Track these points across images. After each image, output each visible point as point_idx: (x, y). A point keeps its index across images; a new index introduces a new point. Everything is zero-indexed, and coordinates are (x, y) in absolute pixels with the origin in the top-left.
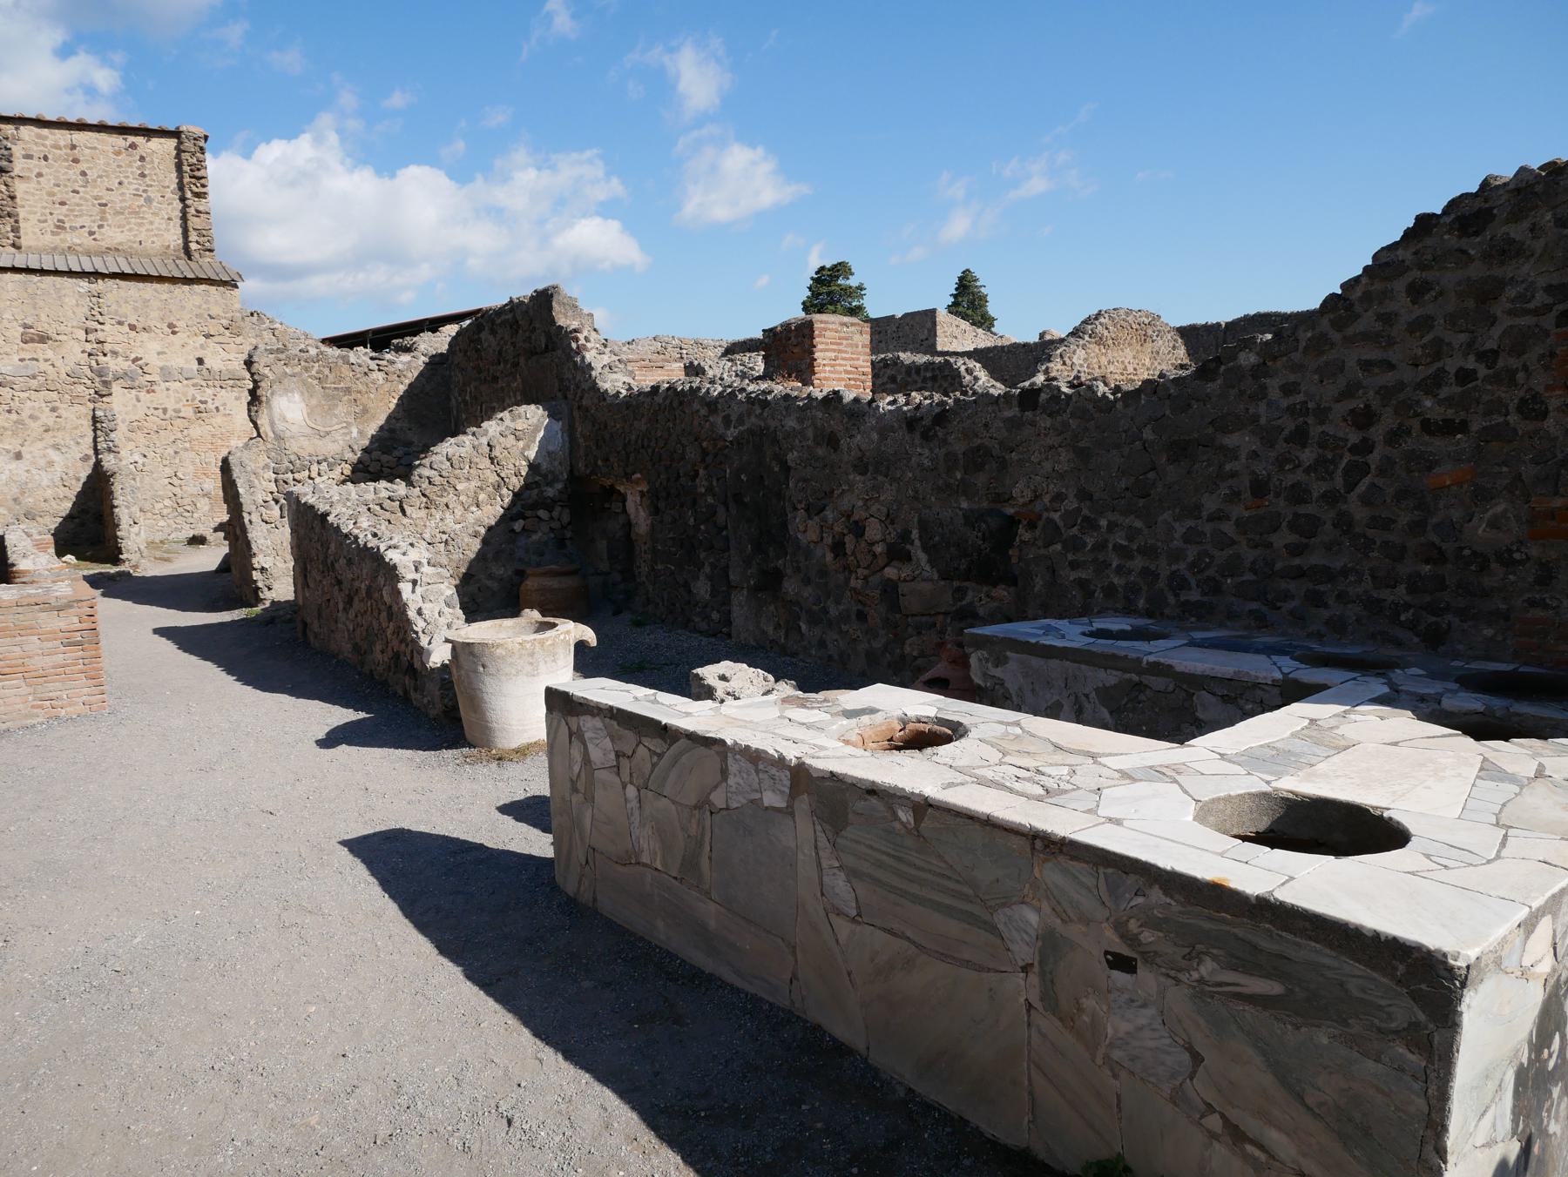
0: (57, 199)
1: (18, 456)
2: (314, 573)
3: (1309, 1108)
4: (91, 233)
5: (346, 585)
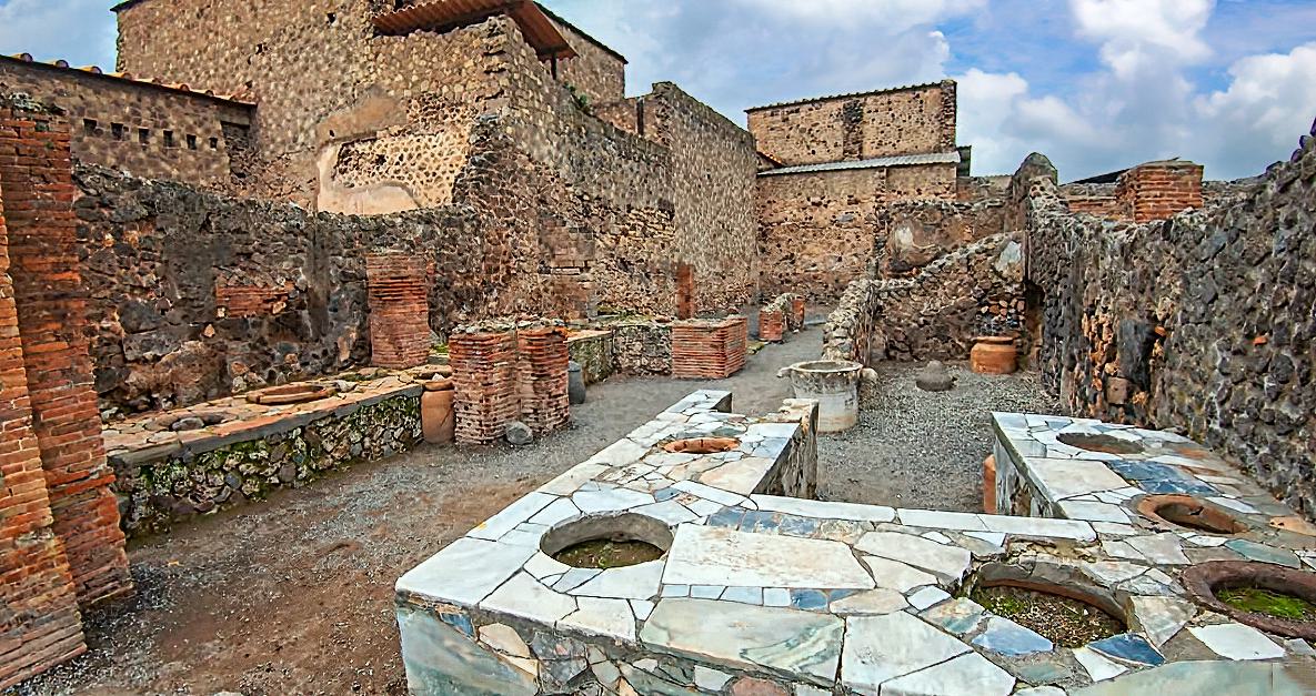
1: (840, 260)
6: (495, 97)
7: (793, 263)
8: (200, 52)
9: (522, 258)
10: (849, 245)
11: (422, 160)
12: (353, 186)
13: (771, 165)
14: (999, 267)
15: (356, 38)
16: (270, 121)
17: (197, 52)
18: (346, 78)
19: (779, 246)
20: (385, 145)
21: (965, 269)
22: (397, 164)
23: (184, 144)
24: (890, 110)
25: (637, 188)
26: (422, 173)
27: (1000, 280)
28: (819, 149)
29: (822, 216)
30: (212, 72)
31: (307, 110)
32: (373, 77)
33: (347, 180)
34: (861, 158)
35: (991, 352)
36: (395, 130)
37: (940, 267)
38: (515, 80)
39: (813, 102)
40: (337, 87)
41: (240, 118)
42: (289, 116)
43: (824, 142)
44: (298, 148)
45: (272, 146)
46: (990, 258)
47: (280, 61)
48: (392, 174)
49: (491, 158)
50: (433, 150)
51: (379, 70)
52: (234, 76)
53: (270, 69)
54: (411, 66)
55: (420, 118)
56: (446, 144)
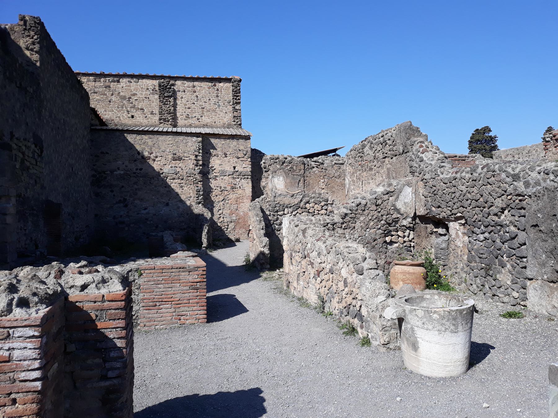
0: (187, 107)
1: (167, 204)
2: (297, 258)
5: (316, 265)
7: (126, 206)
14: (399, 205)
19: (112, 191)
24: (195, 92)
27: (399, 216)
28: (138, 114)
35: (414, 273)
39: (132, 76)
46: (391, 198)
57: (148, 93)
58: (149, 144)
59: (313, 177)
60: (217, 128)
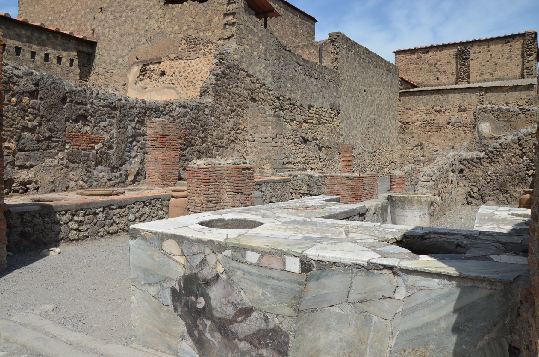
3: (77, 240)
4: (491, 74)
6: (229, 38)
7: (422, 148)
8: (67, 11)
9: (239, 131)
10: (459, 138)
11: (186, 74)
12: (146, 88)
13: (409, 86)
15: (154, 5)
16: (104, 51)
17: (65, 11)
18: (147, 28)
19: (413, 137)
20: (165, 65)
21: (517, 146)
22: (172, 76)
23: (55, 61)
24: (489, 51)
25: (315, 95)
26: (185, 81)
28: (442, 76)
29: (442, 119)
30: (73, 22)
31: (124, 45)
32: (162, 27)
33: (143, 85)
34: (469, 82)
36: (172, 56)
37: (501, 144)
38: (241, 29)
40: (142, 32)
41: (86, 50)
42: (114, 48)
43: (444, 72)
44: (118, 67)
45: (104, 65)
47: (112, 17)
48: (169, 81)
49: (227, 74)
50: (192, 68)
51: (166, 23)
52: (86, 25)
53: (106, 22)
54: (183, 21)
55: (186, 50)
56: (200, 65)
57: (450, 57)
58: (441, 100)
59: (519, 122)
60: (508, 79)
